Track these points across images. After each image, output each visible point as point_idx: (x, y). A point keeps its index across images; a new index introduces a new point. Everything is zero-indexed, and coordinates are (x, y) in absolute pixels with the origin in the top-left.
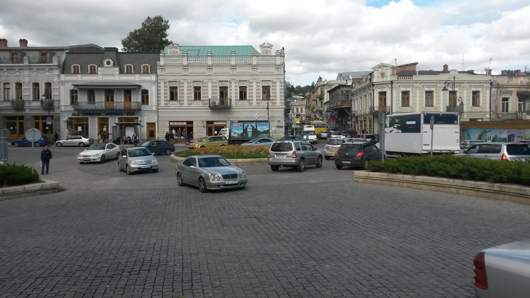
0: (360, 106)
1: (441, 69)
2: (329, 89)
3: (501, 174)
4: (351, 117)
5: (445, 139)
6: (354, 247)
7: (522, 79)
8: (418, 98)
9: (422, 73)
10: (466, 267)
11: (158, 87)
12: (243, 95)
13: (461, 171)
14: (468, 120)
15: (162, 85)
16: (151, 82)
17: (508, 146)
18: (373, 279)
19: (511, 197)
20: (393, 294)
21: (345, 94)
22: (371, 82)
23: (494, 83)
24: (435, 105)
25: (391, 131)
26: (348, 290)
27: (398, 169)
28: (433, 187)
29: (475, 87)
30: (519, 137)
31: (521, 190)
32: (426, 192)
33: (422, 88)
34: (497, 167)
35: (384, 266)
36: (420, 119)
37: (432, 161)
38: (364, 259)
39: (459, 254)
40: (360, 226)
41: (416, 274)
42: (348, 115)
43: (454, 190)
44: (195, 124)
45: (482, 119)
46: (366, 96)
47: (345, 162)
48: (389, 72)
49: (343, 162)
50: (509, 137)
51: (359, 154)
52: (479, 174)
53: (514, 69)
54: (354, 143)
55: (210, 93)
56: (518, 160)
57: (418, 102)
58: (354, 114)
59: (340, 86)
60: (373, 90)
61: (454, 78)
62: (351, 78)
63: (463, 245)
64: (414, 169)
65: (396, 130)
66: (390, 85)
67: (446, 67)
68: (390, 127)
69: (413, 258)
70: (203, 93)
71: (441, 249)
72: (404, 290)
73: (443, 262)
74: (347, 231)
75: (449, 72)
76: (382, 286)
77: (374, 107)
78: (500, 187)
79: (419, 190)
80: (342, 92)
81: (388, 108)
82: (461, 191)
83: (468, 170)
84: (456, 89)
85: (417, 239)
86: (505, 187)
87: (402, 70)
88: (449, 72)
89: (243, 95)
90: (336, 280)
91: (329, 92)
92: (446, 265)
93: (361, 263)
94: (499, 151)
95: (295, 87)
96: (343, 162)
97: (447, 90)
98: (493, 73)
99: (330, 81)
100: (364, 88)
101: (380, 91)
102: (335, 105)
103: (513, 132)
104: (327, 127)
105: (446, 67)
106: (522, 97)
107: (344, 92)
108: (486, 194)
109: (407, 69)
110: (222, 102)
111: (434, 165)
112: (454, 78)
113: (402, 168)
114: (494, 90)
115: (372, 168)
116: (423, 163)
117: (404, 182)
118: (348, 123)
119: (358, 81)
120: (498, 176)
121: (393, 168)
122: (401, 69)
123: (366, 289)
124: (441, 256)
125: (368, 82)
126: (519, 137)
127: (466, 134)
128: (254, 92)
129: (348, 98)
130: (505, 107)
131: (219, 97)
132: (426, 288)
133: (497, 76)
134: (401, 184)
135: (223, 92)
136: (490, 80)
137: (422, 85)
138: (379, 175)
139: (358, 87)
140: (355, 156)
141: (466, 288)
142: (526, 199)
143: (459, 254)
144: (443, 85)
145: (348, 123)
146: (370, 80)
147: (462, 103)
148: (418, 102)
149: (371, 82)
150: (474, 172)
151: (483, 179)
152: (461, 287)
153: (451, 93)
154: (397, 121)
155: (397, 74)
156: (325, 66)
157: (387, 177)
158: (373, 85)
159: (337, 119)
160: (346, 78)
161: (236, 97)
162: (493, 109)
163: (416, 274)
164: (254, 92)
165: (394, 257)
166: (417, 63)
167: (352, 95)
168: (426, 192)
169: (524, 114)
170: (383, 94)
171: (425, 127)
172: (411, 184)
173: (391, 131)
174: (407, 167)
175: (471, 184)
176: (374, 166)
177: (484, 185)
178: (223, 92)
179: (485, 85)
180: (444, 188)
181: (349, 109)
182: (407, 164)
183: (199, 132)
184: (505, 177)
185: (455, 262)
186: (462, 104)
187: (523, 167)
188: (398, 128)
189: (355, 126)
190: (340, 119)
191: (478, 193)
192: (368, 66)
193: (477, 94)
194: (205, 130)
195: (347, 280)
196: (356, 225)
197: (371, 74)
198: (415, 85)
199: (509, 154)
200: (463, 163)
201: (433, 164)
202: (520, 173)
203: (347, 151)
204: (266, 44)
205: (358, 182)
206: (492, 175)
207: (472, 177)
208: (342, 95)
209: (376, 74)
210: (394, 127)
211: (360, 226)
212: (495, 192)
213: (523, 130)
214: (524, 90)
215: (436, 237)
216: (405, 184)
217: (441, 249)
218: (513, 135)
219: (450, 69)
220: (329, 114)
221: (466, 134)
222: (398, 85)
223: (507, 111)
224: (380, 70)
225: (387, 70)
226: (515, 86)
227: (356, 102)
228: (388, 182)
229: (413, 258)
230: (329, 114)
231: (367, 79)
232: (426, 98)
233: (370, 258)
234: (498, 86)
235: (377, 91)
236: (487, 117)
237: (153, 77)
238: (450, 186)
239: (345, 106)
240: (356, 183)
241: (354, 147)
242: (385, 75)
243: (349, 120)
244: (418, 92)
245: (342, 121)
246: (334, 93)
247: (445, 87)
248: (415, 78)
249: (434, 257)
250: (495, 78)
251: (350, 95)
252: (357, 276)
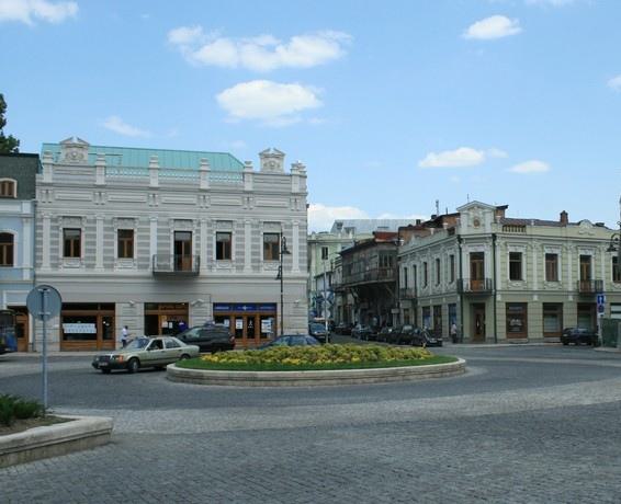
1: (557, 219)
11: (36, 228)
12: (223, 250)
15: (47, 225)
16: (21, 217)
44: (119, 310)
48: (489, 218)
55: (154, 245)
60: (460, 249)
67: (564, 215)
70: (140, 237)
89: (223, 250)
105: (564, 215)
110: (178, 263)
128: (247, 244)
131: (172, 253)
135: (182, 248)
158: (460, 240)
161: (210, 253)
164: (247, 244)
166: (506, 207)
170: (477, 258)
178: (182, 248)
181: (394, 284)
183: (130, 323)
194: (141, 322)
204: (272, 152)
209: (464, 219)
219: (571, 219)
225: (484, 213)
235: (467, 250)
237: (26, 207)
242: (482, 223)
243: (393, 307)
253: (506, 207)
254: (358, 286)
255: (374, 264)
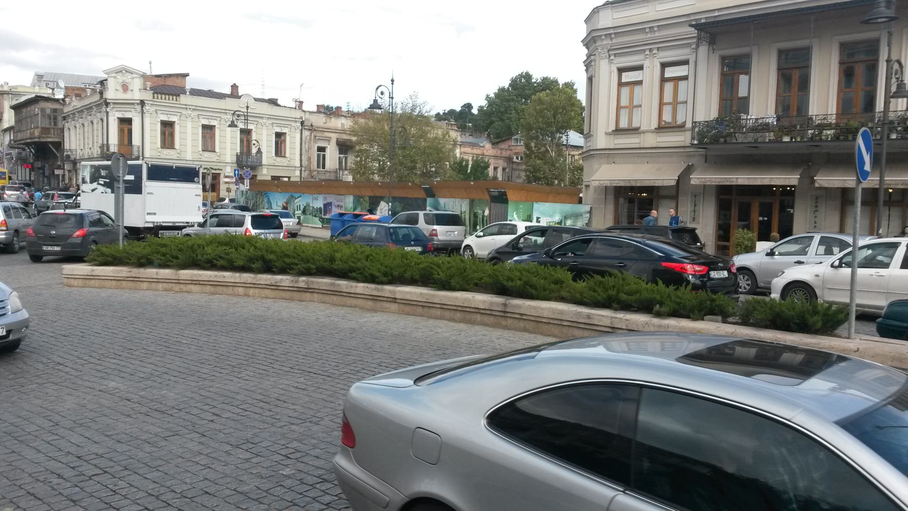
0: (79, 141)
1: (228, 91)
2: (14, 102)
3: (308, 262)
4: (63, 161)
5: (173, 206)
6: (51, 411)
7: (343, 120)
8: (189, 136)
9: (195, 93)
10: (248, 413)
13: (251, 260)
14: (270, 178)
17: (253, 217)
18: (84, 463)
19: (321, 296)
20: (120, 483)
21: (49, 117)
22: (101, 97)
23: (306, 124)
24: (217, 150)
25: (93, 190)
26: (32, 495)
27: (148, 259)
28: (209, 288)
29: (279, 126)
30: (338, 206)
31: (93, 270)
32: (197, 297)
33: (196, 119)
34: (304, 252)
35: (107, 436)
36: (141, 172)
37: (208, 245)
38: (70, 429)
39: (238, 393)
40: (67, 369)
41: (165, 439)
42: (56, 157)
43: (241, 290)
45: (289, 178)
46: (92, 122)
47: (50, 248)
48: (137, 84)
49: (45, 248)
50: (325, 205)
51: (78, 233)
52: (277, 264)
53: (334, 104)
54: (68, 211)
56: (262, 236)
57: (189, 143)
58: (68, 156)
59: (37, 99)
60: (107, 113)
61: (247, 107)
62: (62, 84)
63: (247, 378)
64: (177, 258)
65: (101, 189)
66: (139, 108)
67: (234, 87)
68: (91, 182)
69: (163, 412)
71: (211, 389)
72: (141, 472)
73: (213, 410)
74: (39, 381)
75: (239, 97)
76: (101, 472)
77: (108, 146)
78: (307, 283)
79: (185, 294)
80: (43, 110)
81: (135, 149)
82: (251, 291)
83: (262, 258)
84: (250, 127)
85: (173, 378)
86: (313, 282)
87: (161, 83)
88: (239, 97)
90: (5, 480)
91: (16, 108)
92: (217, 415)
93: (63, 438)
94: (240, 224)
95: (507, 86)
96: (45, 248)
97: (236, 126)
98: (305, 107)
99: (16, 87)
100: (89, 108)
101: (121, 116)
102: (27, 134)
103: (331, 199)
104: (10, 178)
105: (234, 87)
106: (344, 147)
107: (48, 111)
108: (288, 294)
109: (169, 82)
111: (210, 251)
112: (247, 107)
113: (156, 258)
114: (306, 133)
115: (99, 259)
116: (192, 247)
117: (158, 281)
118: (57, 172)
119: (77, 92)
120: (304, 266)
121: (139, 259)
122: (161, 82)
123: (69, 485)
124: (209, 401)
125: (97, 97)
126: (338, 206)
127: (266, 200)
129: (55, 124)
130: (322, 162)
132: (180, 460)
133: (310, 112)
134: (154, 285)
136: (301, 118)
137: (196, 113)
138: (113, 271)
139: (76, 103)
140: (70, 236)
141: (244, 447)
142: (340, 298)
143: (238, 393)
144: (229, 117)
145: (57, 172)
146: (101, 93)
147: (259, 149)
148: (189, 143)
149: (101, 97)
150: (270, 261)
151: (283, 271)
152: (237, 447)
153: (243, 131)
154: (103, 173)
155: (151, 89)
156: (14, 54)
157: (129, 275)
158: (107, 104)
159: (32, 164)
160: (51, 85)
162: (305, 163)
163: (165, 439)
165: (129, 416)
166: (187, 75)
167: (64, 118)
168: (197, 297)
169: (346, 172)
170: (126, 122)
171: (148, 185)
172: (171, 285)
173: (93, 190)
174: (164, 255)
175: (266, 280)
176: (103, 254)
177: (285, 280)
179: (293, 124)
180: (225, 289)
181: (59, 145)
182: (163, 250)
184: (313, 267)
185: (230, 408)
186: (259, 152)
187: (337, 252)
188: (105, 185)
189: (70, 179)
190: (38, 164)
191: (276, 292)
192: (92, 68)
193: (283, 138)
195: (30, 475)
196: (61, 367)
197: (102, 83)
198: (184, 112)
199: (254, 228)
200: (256, 247)
201: (209, 250)
202: (332, 260)
203: (54, 227)
205: (70, 286)
206: (297, 265)
207: (268, 268)
208: (43, 116)
210: (99, 184)
211: (67, 369)
212: (300, 290)
213: (342, 197)
214: (345, 137)
215: (206, 371)
216: (160, 285)
217: (211, 389)
218: (330, 204)
220: (14, 152)
221: (266, 200)
222: (153, 109)
223: (324, 167)
224: (120, 78)
225: (133, 78)
226: (335, 131)
227: (72, 131)
228: (130, 284)
229: (163, 412)
230: (14, 152)
231: (94, 91)
232: (204, 137)
233: (81, 425)
234: (312, 129)
236: (296, 176)
238: (235, 285)
239: (50, 140)
240: (66, 288)
241: (68, 219)
242: (130, 88)
243: (59, 168)
244: (189, 124)
245: (43, 168)
246: (24, 110)
247: (233, 122)
248: (185, 99)
249: (199, 405)
250: (307, 116)
251: (60, 119)
252: (53, 465)
253: (187, 75)
254: (35, 143)
255: (41, 122)
